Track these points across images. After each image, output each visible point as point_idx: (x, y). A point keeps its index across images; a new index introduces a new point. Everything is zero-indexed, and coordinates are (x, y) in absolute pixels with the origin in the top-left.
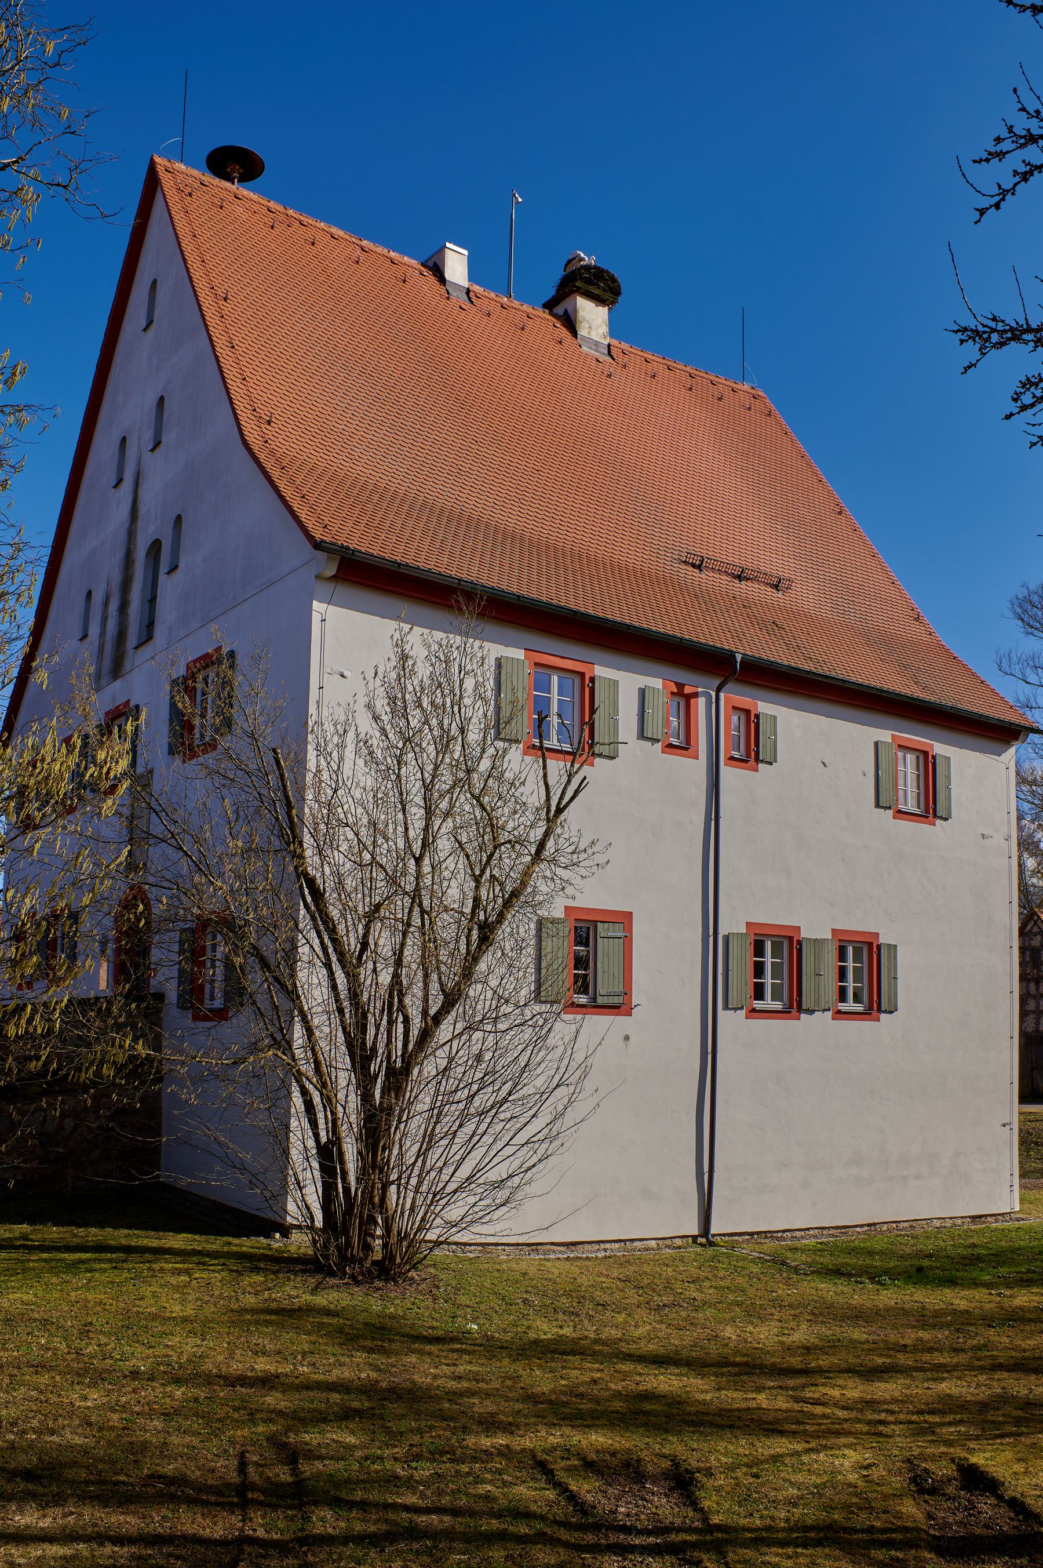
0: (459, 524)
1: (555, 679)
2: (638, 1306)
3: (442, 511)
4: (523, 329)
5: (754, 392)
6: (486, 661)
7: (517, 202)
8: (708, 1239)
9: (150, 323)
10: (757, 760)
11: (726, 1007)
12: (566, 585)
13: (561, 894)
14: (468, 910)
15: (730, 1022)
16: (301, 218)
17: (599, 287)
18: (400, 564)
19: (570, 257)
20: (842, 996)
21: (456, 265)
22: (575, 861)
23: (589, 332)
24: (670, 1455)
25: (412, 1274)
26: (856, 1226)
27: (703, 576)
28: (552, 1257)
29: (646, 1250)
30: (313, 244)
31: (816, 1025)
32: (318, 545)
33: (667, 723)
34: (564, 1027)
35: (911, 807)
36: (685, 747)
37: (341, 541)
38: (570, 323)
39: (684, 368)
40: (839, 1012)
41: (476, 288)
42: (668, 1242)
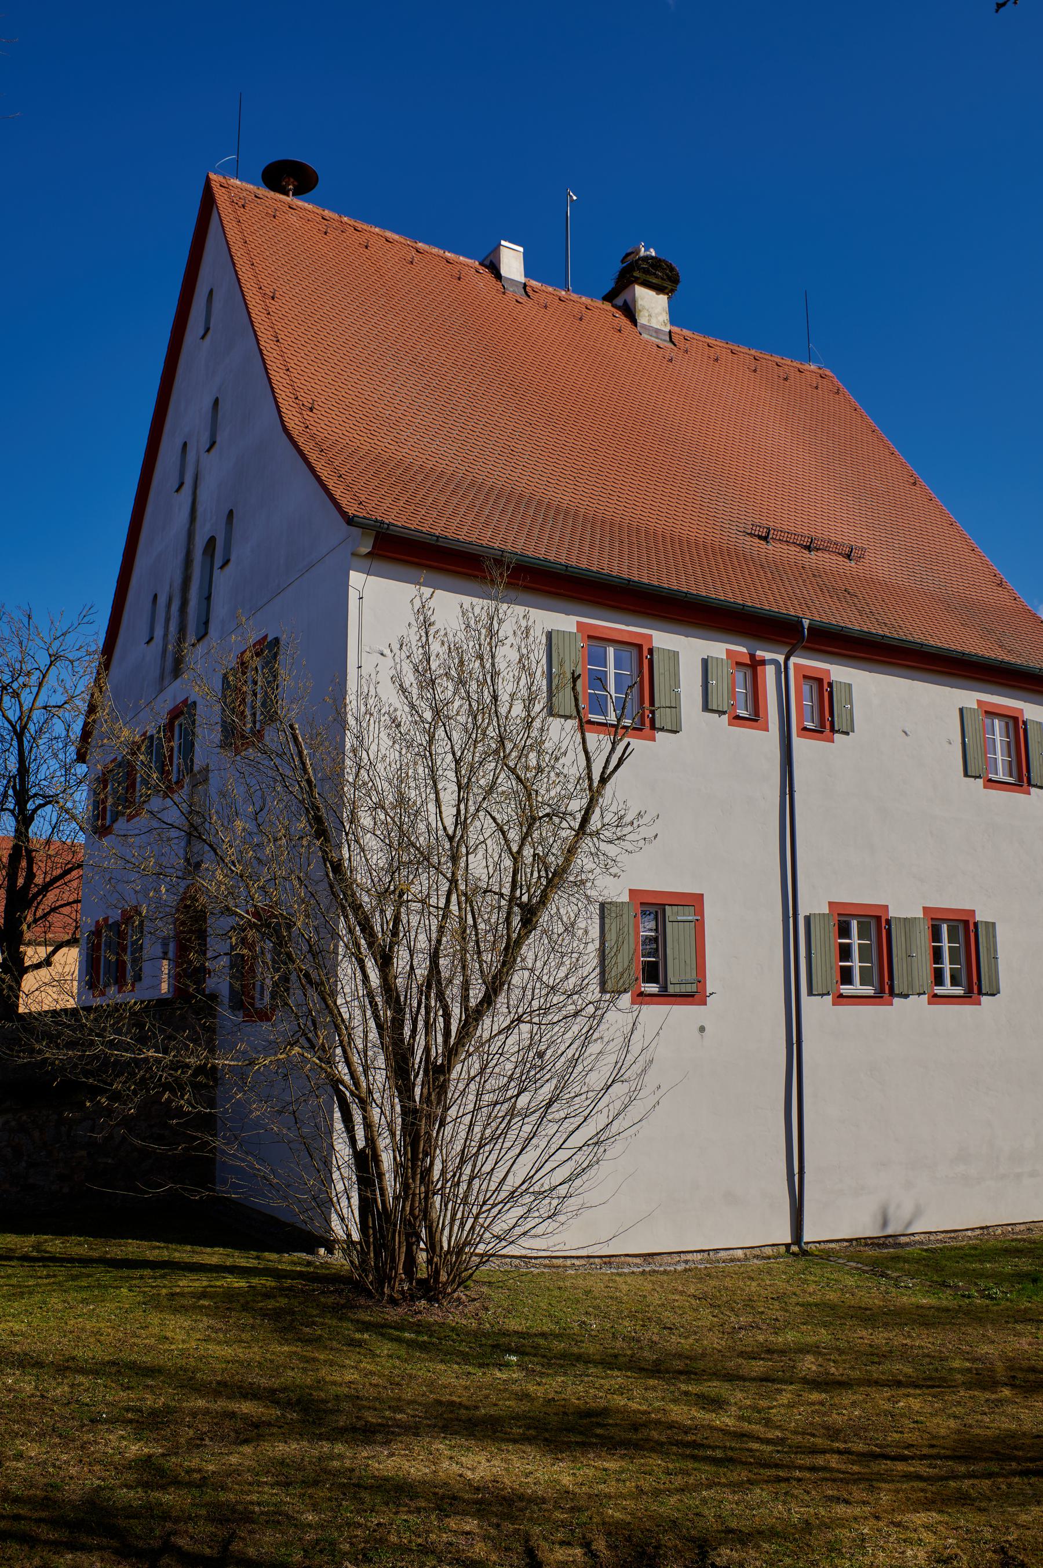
0: (508, 501)
1: (611, 651)
2: (710, 1330)
3: (491, 489)
4: (581, 319)
5: (821, 372)
6: (532, 632)
7: (572, 200)
8: (800, 1247)
9: (207, 330)
10: (833, 730)
11: (810, 993)
12: (621, 556)
13: (615, 874)
14: (506, 891)
15: (816, 1010)
16: (356, 224)
17: (657, 277)
18: (438, 537)
19: (629, 251)
20: (938, 979)
21: (512, 261)
22: (619, 834)
23: (649, 321)
24: (699, 1539)
25: (459, 1294)
26: (967, 1230)
27: (770, 547)
28: (626, 1271)
29: (732, 1260)
30: (366, 247)
31: (911, 1011)
32: (350, 521)
33: (733, 694)
34: (620, 1015)
35: (1001, 776)
36: (755, 718)
37: (377, 515)
38: (630, 312)
39: (748, 351)
40: (935, 996)
41: (534, 283)
42: (757, 1252)
